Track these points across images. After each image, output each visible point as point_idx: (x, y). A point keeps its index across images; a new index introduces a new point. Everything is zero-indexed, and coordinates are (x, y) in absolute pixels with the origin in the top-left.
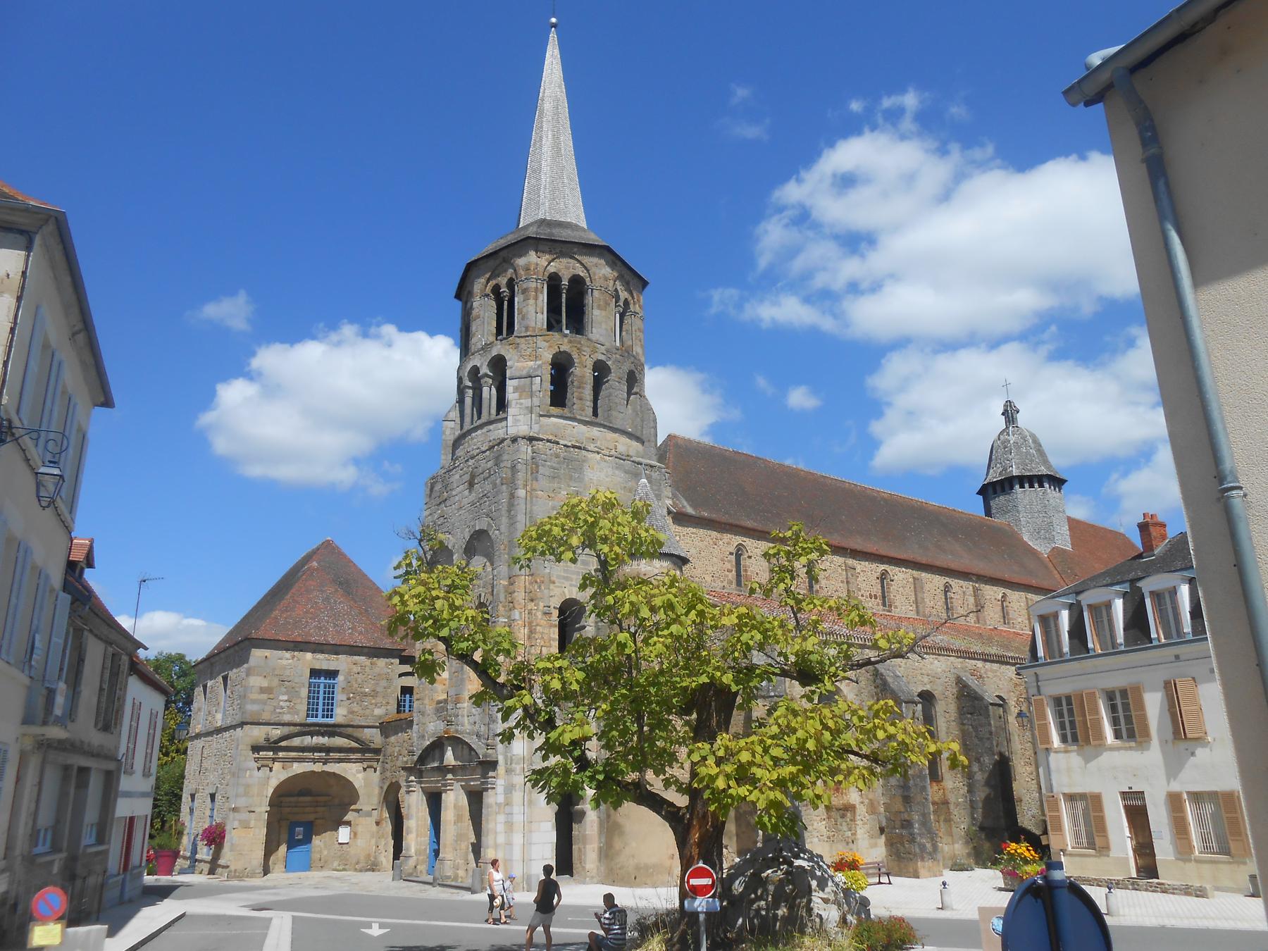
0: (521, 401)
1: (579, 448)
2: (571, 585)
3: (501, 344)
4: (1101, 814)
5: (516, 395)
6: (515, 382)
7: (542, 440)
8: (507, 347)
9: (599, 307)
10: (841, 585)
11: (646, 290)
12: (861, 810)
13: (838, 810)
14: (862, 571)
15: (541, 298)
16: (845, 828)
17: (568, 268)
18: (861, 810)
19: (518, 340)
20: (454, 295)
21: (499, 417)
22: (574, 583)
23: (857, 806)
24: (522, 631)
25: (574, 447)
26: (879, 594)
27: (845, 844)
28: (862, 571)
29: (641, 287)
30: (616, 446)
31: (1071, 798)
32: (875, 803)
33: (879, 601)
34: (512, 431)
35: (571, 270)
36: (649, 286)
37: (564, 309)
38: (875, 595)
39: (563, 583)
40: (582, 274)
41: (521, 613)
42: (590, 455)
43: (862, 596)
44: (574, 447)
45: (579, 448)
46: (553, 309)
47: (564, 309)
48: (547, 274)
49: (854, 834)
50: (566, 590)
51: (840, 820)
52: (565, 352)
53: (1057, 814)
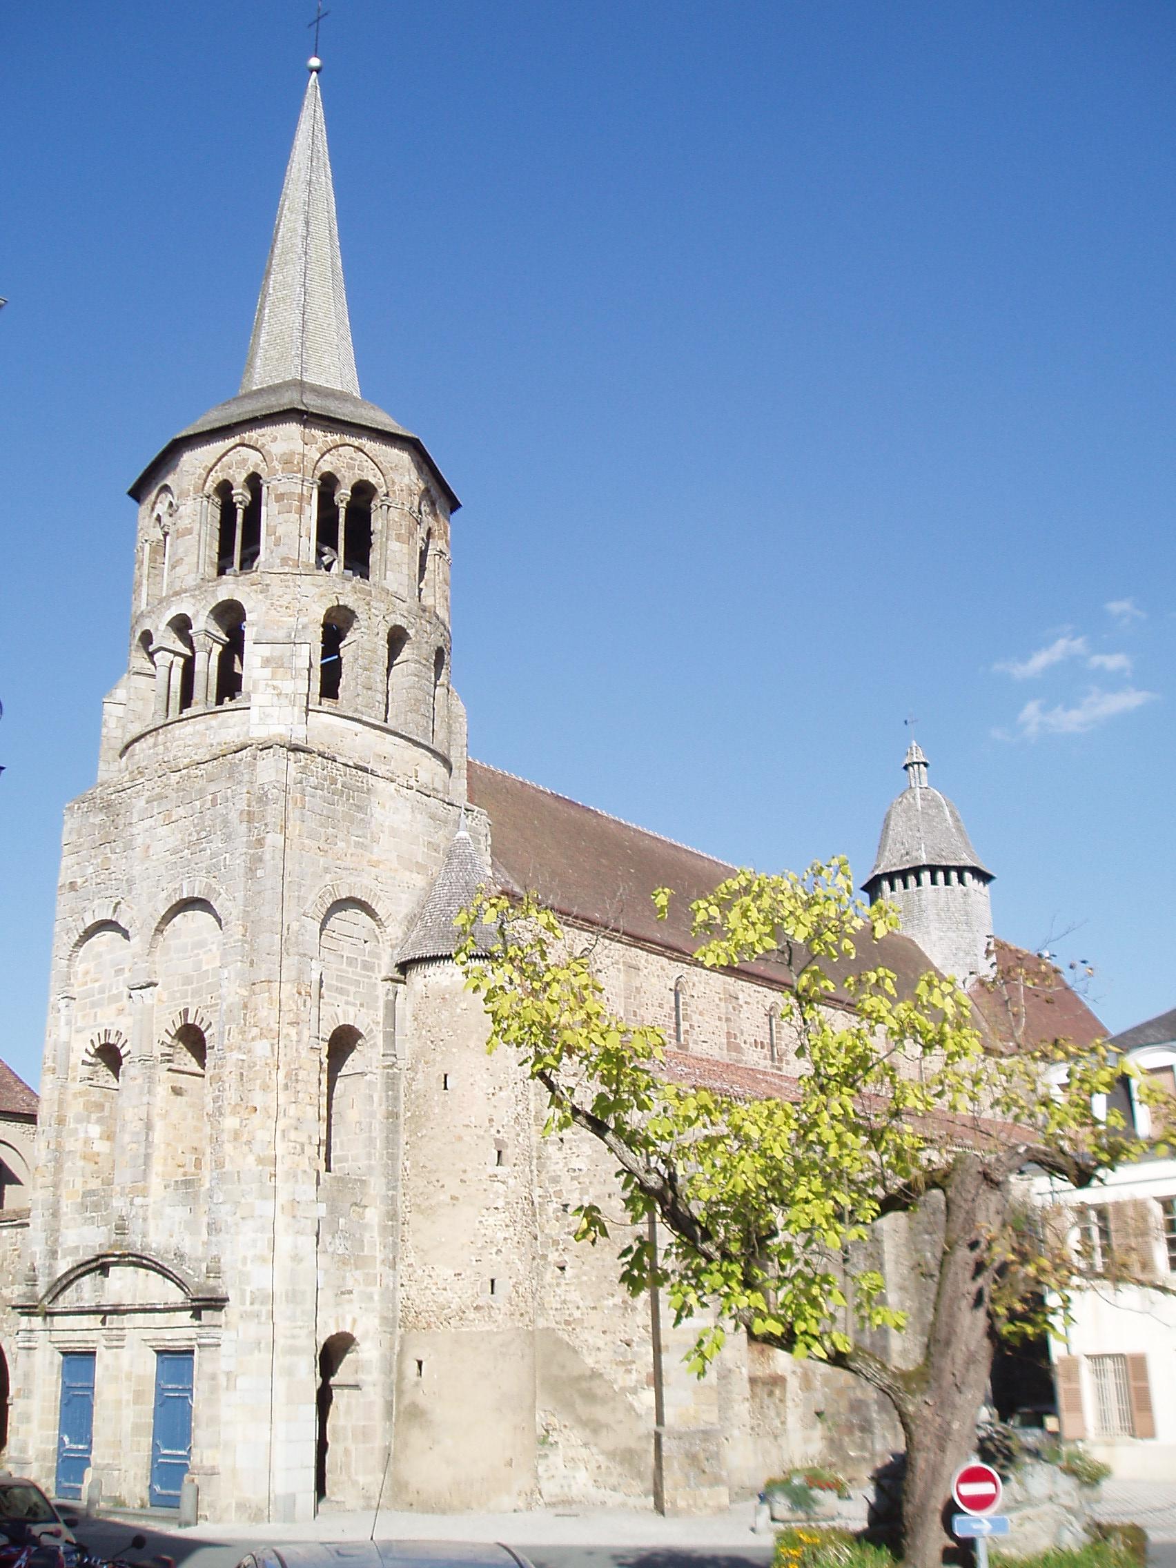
0: (275, 683)
1: (365, 770)
2: (347, 1003)
3: (236, 583)
4: (1074, 1386)
5: (267, 672)
6: (265, 650)
7: (310, 752)
8: (247, 589)
9: (399, 537)
10: (718, 1023)
11: (455, 514)
12: (793, 1384)
13: (765, 1383)
14: (746, 1003)
15: (307, 513)
16: (772, 1413)
17: (350, 467)
18: (793, 1384)
19: (268, 579)
20: (129, 487)
21: (184, 716)
22: (351, 999)
23: (789, 1379)
24: (274, 1076)
25: (357, 767)
26: (766, 1041)
27: (772, 1439)
28: (746, 1003)
29: (449, 511)
30: (416, 771)
31: (1096, 1358)
32: (810, 1374)
33: (766, 1051)
34: (260, 733)
35: (356, 471)
36: (459, 511)
37: (341, 535)
38: (762, 1043)
39: (336, 999)
40: (373, 481)
41: (272, 1045)
42: (381, 784)
43: (745, 1042)
44: (357, 767)
45: (365, 770)
46: (326, 535)
47: (341, 535)
48: (318, 474)
49: (783, 1423)
50: (339, 1011)
51: (767, 1400)
52: (345, 607)
53: (177, 1493)
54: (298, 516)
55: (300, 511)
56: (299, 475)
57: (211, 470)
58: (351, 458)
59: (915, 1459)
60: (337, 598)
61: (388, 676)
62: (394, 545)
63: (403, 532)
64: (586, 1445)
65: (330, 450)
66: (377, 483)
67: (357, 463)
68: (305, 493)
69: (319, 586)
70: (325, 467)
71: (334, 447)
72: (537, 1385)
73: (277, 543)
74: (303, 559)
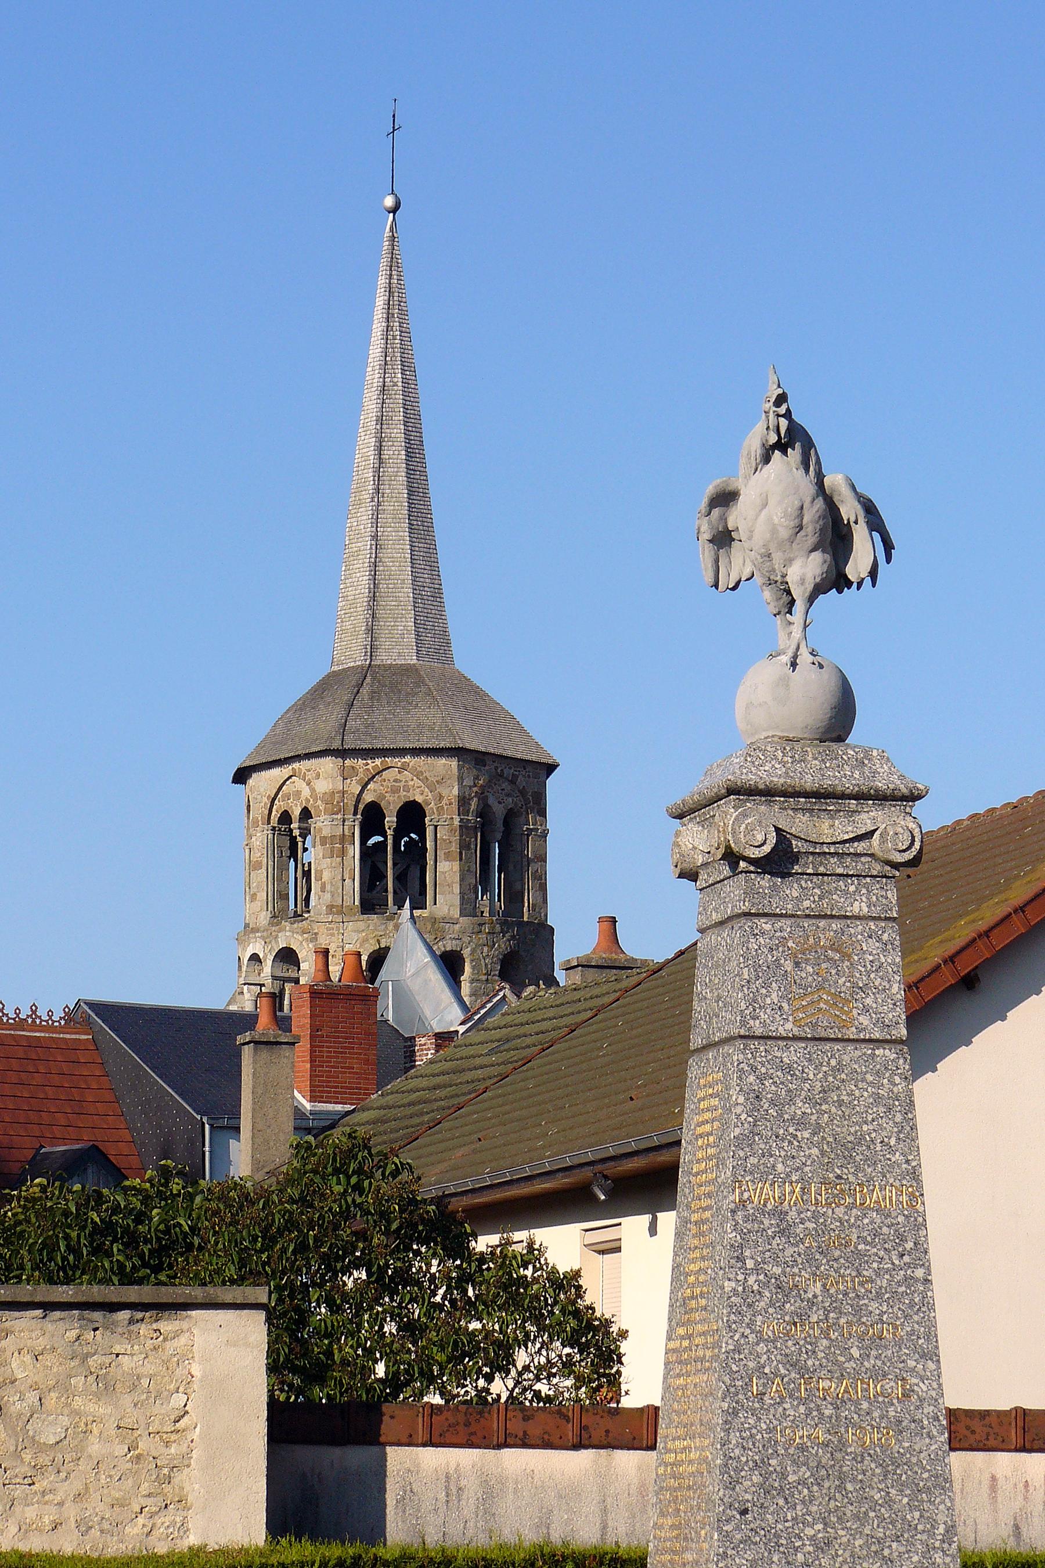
19: (315, 926)
40: (419, 799)
54: (339, 859)
55: (343, 853)
56: (339, 816)
57: (274, 800)
58: (396, 781)
59: (566, 1544)
60: (378, 941)
61: (875, 557)
62: (443, 866)
63: (453, 849)
64: (856, 1049)
65: (374, 777)
66: (425, 801)
67: (403, 783)
68: (346, 833)
69: (359, 932)
70: (368, 797)
71: (378, 773)
72: (496, 1435)
73: (323, 889)
74: (348, 902)
